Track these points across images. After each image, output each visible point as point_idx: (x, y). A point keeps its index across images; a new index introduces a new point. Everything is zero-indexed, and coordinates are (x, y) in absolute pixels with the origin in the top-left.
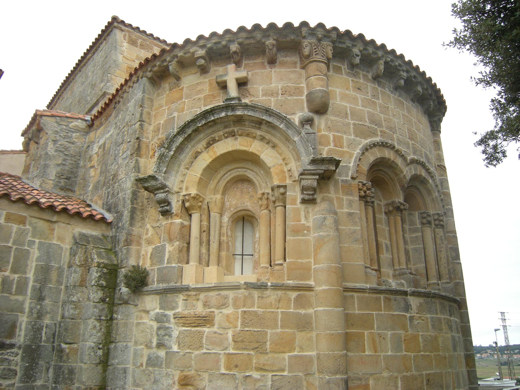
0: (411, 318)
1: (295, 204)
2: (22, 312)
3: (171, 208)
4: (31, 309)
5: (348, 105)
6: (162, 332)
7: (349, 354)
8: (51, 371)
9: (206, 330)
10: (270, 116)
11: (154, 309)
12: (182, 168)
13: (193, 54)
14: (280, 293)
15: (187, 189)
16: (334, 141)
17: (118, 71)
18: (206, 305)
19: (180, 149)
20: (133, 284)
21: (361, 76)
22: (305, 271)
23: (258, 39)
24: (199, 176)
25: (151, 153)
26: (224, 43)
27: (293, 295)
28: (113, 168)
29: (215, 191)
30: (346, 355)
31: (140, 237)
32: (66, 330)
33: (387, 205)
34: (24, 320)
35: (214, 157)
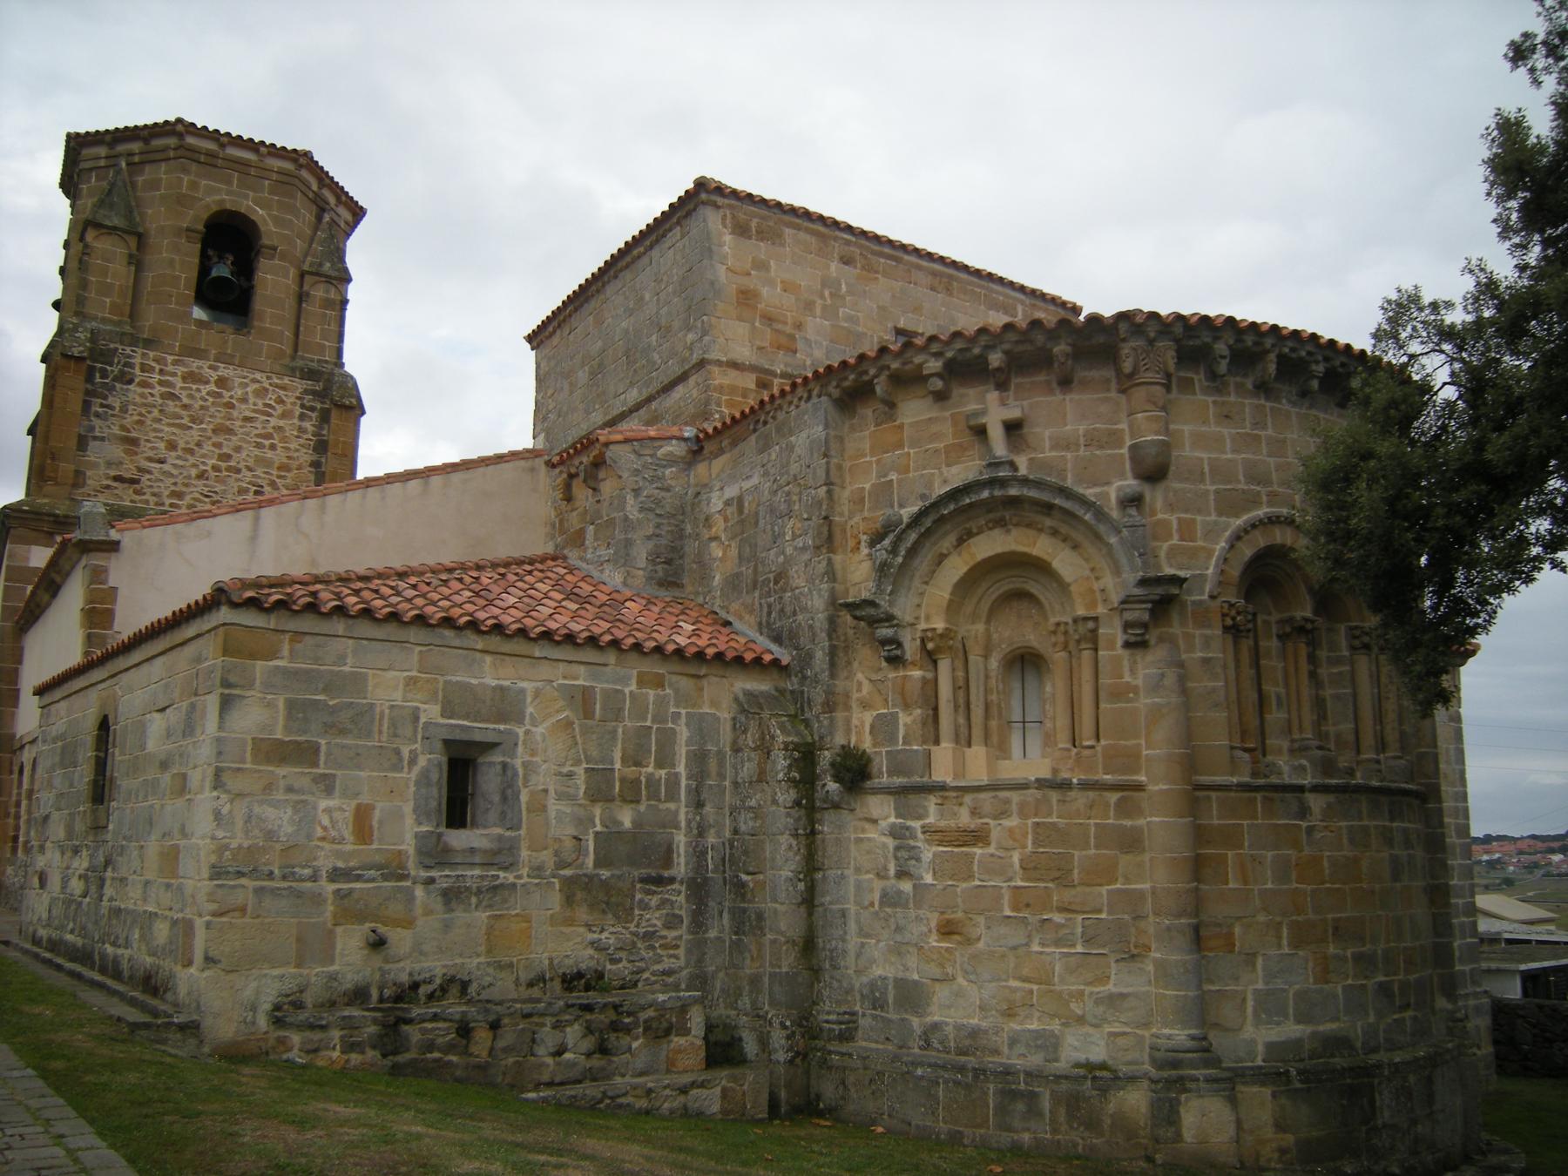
0: (1310, 830)
1: (1113, 648)
2: (677, 827)
3: (904, 652)
4: (689, 822)
5: (1204, 455)
6: (904, 854)
7: (1202, 886)
8: (726, 915)
9: (978, 851)
10: (1067, 498)
11: (886, 818)
12: (917, 582)
13: (920, 366)
14: (1091, 794)
15: (928, 618)
16: (1179, 530)
17: (721, 305)
18: (974, 812)
19: (912, 552)
20: (848, 776)
21: (1232, 388)
22: (1132, 760)
23: (1039, 344)
24: (947, 596)
25: (851, 543)
26: (976, 351)
27: (1113, 797)
28: (774, 559)
29: (974, 618)
30: (1197, 889)
31: (847, 696)
32: (746, 853)
33: (1281, 622)
34: (681, 840)
35: (972, 564)
